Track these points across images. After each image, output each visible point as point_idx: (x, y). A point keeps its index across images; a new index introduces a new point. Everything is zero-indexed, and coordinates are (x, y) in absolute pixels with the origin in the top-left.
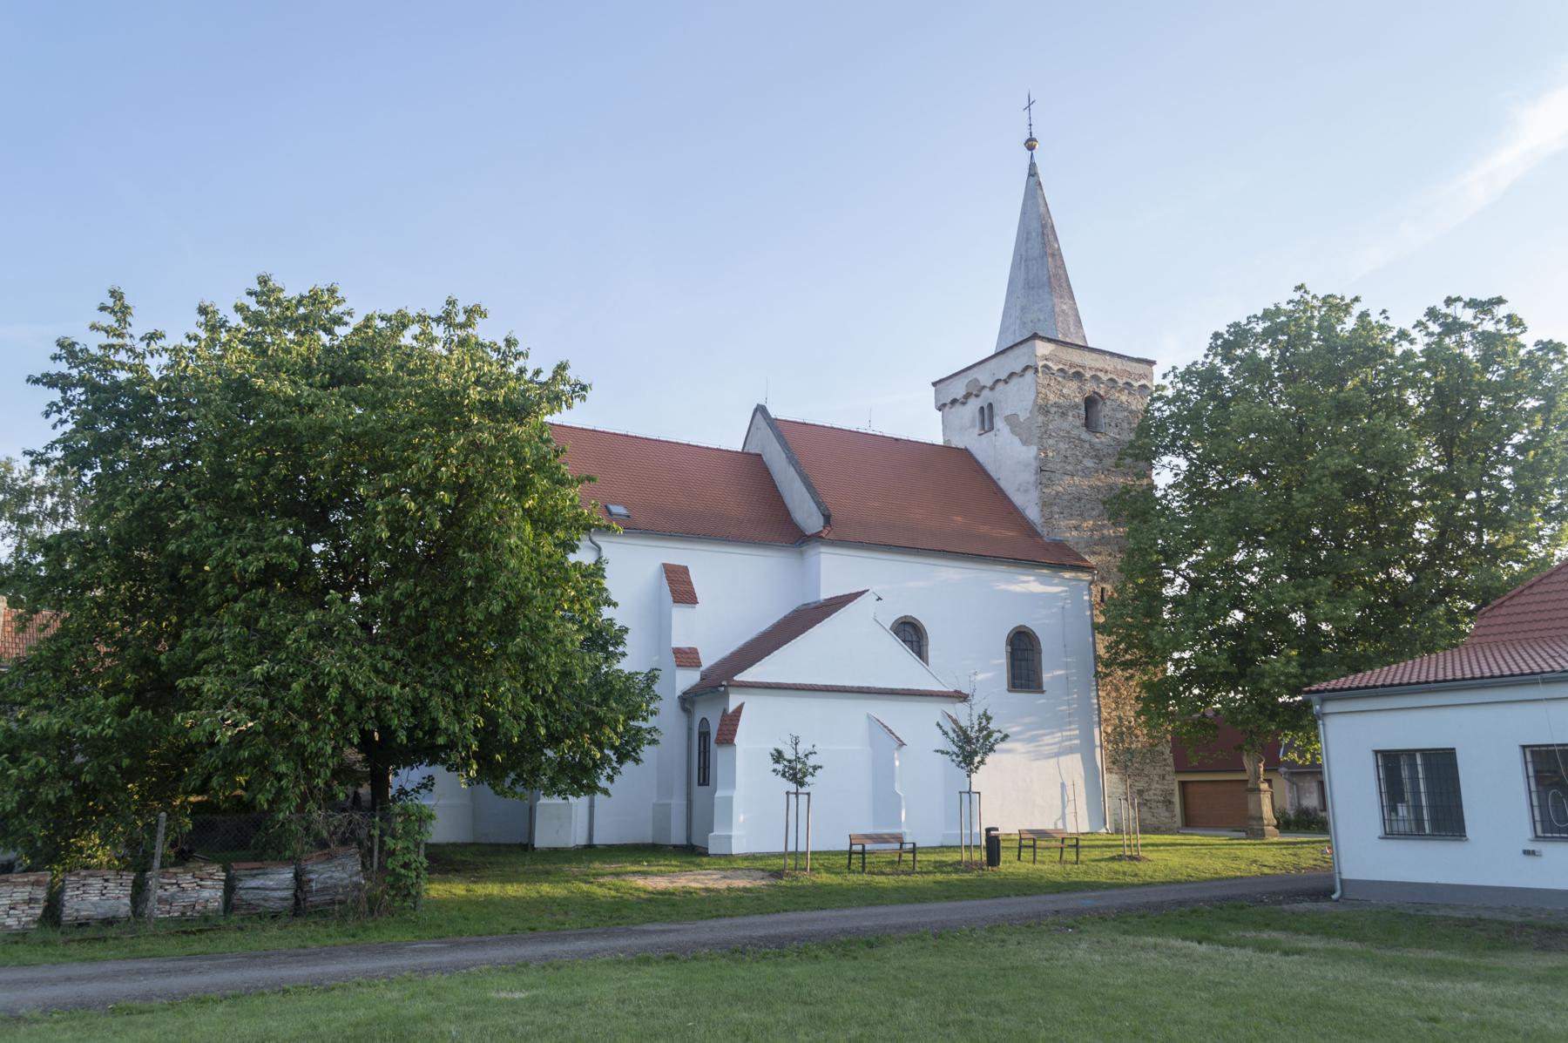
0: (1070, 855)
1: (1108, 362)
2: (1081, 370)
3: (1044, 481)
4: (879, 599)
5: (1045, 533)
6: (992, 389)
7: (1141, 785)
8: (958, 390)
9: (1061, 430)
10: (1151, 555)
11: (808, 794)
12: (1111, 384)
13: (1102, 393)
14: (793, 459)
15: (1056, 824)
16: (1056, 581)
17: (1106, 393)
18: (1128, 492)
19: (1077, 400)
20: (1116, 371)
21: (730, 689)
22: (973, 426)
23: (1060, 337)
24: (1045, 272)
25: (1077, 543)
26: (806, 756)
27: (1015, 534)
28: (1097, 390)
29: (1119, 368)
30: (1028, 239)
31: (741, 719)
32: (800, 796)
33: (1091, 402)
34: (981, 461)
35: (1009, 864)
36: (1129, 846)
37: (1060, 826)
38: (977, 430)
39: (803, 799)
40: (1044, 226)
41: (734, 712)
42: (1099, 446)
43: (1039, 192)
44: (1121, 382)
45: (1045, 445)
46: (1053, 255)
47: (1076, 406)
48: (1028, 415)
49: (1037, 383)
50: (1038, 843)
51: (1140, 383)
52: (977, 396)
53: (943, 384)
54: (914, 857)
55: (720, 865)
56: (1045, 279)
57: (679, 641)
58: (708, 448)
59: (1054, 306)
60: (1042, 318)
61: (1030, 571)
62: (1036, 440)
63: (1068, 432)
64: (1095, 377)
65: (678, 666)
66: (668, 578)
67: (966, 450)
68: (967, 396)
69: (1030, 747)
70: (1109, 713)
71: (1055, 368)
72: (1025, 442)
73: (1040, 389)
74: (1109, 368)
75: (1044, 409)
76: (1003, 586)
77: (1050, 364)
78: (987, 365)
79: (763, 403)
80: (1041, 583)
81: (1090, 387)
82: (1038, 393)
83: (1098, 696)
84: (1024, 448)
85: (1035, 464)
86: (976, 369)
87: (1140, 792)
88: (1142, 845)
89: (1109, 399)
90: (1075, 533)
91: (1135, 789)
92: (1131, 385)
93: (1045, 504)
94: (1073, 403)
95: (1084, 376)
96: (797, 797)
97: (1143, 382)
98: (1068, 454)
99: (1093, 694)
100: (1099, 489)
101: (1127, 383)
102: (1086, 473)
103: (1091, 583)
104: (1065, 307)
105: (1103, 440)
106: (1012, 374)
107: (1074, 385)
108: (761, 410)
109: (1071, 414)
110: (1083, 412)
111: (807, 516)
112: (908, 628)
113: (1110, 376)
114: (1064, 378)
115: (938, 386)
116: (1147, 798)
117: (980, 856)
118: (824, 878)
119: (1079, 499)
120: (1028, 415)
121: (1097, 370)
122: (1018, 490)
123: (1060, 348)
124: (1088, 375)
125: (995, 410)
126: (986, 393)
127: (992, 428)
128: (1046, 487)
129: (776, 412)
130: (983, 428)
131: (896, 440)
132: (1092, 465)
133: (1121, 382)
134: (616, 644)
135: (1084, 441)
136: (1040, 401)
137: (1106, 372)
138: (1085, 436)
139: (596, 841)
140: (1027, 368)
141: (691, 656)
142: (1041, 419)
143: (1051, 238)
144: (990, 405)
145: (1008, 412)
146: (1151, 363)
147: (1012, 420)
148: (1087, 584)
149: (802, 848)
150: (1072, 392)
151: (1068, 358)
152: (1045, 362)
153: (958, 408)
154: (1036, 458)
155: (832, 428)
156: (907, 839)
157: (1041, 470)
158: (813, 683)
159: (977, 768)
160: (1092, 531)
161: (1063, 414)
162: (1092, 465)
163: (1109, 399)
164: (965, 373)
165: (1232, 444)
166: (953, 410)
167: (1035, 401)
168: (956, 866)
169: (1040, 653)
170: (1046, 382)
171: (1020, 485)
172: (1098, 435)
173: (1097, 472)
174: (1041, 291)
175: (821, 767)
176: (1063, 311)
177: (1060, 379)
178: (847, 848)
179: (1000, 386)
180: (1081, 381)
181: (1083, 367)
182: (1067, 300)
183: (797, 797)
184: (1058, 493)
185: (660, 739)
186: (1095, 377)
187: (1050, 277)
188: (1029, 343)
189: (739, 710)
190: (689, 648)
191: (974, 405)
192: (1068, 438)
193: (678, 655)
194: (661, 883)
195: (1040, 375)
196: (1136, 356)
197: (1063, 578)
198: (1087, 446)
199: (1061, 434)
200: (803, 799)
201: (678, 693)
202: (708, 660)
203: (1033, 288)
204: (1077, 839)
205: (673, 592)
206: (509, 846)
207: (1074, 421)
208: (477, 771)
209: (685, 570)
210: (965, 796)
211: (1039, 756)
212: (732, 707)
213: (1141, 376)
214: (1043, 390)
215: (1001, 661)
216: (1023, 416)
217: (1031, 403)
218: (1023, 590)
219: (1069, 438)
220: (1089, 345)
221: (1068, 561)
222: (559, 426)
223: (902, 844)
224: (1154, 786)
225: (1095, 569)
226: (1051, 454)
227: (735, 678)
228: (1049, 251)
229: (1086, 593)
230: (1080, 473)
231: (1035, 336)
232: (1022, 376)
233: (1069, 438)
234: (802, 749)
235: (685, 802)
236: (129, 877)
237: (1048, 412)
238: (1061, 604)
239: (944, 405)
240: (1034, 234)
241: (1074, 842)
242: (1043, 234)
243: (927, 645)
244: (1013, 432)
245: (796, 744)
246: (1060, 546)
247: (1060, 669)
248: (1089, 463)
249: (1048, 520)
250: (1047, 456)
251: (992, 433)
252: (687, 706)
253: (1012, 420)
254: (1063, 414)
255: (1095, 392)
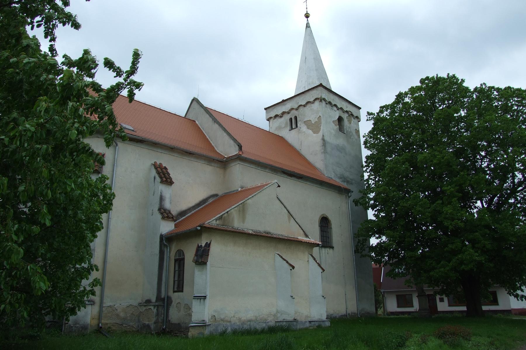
4: (279, 186)
6: (297, 109)
38: (289, 128)
122: (312, 154)
126: (294, 112)
144: (296, 118)
165: (429, 133)
179: (301, 109)
191: (287, 117)
236: (312, 322)
239: (271, 118)
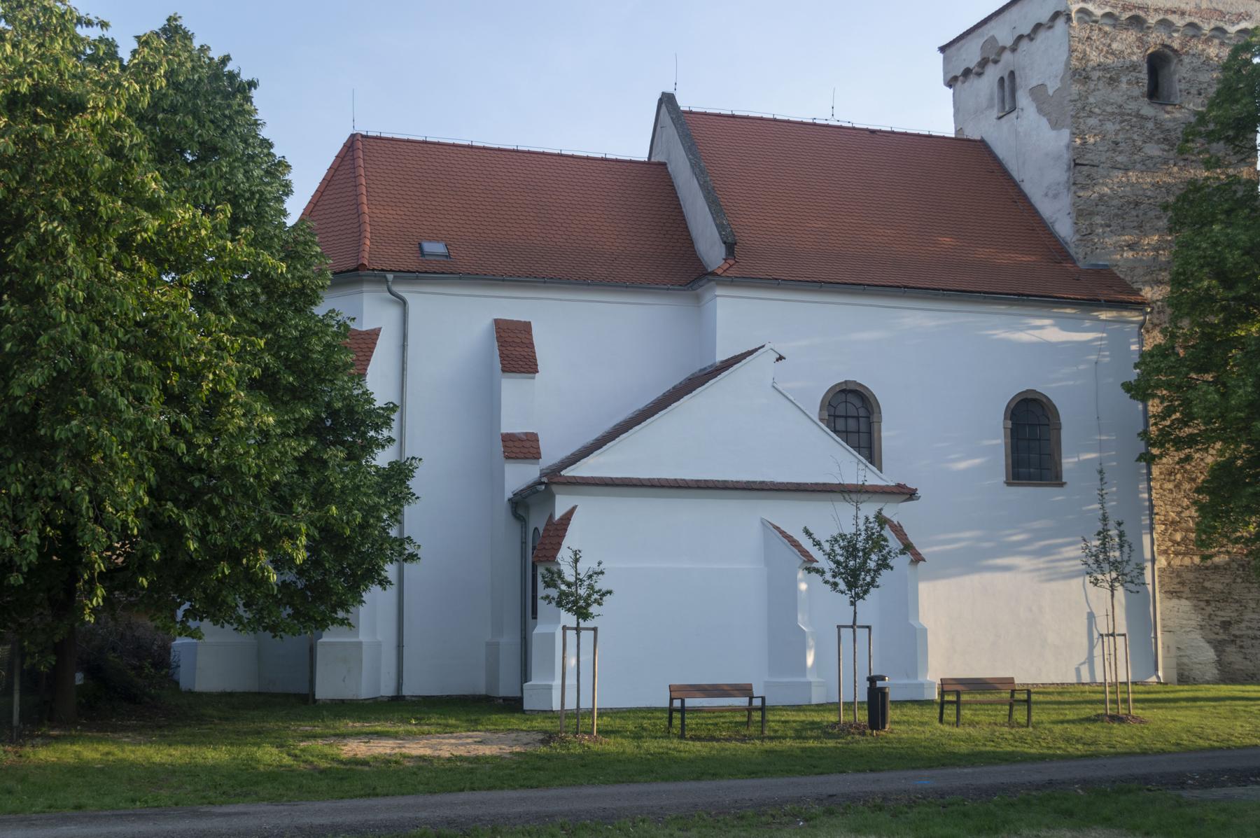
0: (1020, 715)
2: (1141, 13)
3: (1080, 180)
4: (781, 358)
5: (1081, 257)
6: (1014, 49)
7: (1228, 613)
8: (971, 55)
9: (1108, 104)
11: (595, 629)
12: (1191, 32)
13: (1176, 45)
14: (698, 169)
15: (1078, 670)
16: (1088, 324)
17: (1183, 45)
18: (1198, 189)
19: (1135, 58)
21: (554, 488)
22: (990, 106)
25: (1132, 269)
26: (590, 577)
27: (1033, 258)
28: (1168, 42)
31: (570, 528)
32: (583, 633)
33: (1158, 63)
34: (1001, 157)
35: (899, 727)
36: (1112, 702)
37: (1086, 678)
38: (995, 113)
39: (587, 636)
41: (561, 519)
42: (1171, 125)
44: (1207, 28)
45: (1082, 127)
47: (1134, 67)
49: (1070, 37)
50: (964, 698)
51: (1238, 28)
52: (996, 62)
53: (953, 49)
54: (763, 716)
55: (334, 728)
57: (511, 424)
58: (588, 158)
61: (1045, 311)
62: (1069, 121)
63: (1120, 106)
64: (1164, 23)
65: (507, 458)
66: (499, 339)
67: (982, 142)
68: (984, 63)
69: (1040, 562)
70: (1179, 514)
71: (1098, 12)
72: (1055, 125)
73: (1075, 44)
74: (1187, 8)
75: (1080, 75)
79: (670, 90)
80: (1064, 329)
81: (1155, 39)
82: (1072, 51)
83: (1150, 489)
84: (1054, 133)
85: (1066, 156)
87: (1226, 625)
88: (1135, 701)
90: (1129, 254)
91: (1218, 620)
93: (1082, 213)
94: (1128, 64)
95: (1145, 21)
96: (578, 634)
98: (1120, 137)
99: (1143, 486)
100: (1168, 188)
102: (1149, 165)
103: (1142, 325)
105: (1178, 115)
106: (1038, 26)
107: (1131, 36)
108: (667, 101)
109: (1124, 79)
110: (1144, 76)
111: (711, 249)
112: (851, 398)
113: (1188, 19)
114: (1114, 26)
116: (1237, 633)
117: (862, 716)
118: (611, 745)
119: (1137, 204)
120: (1059, 85)
121: (1167, 11)
124: (1152, 20)
125: (1018, 80)
126: (1007, 56)
127: (1013, 109)
128: (1083, 188)
129: (684, 103)
130: (1004, 107)
131: (873, 132)
133: (1207, 28)
134: (377, 428)
135: (1147, 119)
136: (1074, 62)
137: (1183, 13)
138: (1148, 110)
139: (406, 692)
140: (1056, 15)
141: (527, 444)
142: (1076, 88)
144: (1012, 74)
145: (1034, 83)
147: (1038, 93)
149: (586, 704)
150: (1127, 45)
154: (1068, 147)
156: (757, 692)
157: (1076, 164)
158: (678, 477)
159: (866, 592)
161: (1113, 81)
164: (980, 30)
167: (1068, 63)
168: (827, 731)
169: (1059, 429)
170: (1084, 34)
172: (1169, 108)
175: (610, 592)
177: (1107, 29)
178: (667, 704)
179: (1024, 44)
180: (1142, 30)
181: (1145, 9)
183: (578, 634)
184: (1102, 196)
185: (420, 553)
186: (1164, 23)
189: (567, 517)
190: (526, 434)
191: (993, 74)
192: (1121, 114)
193: (510, 444)
194: (383, 748)
195: (1075, 23)
197: (1098, 319)
198: (1150, 125)
199: (1109, 109)
200: (587, 636)
201: (508, 494)
202: (551, 454)
204: (1029, 692)
205: (503, 357)
206: (287, 696)
207: (1131, 91)
208: (104, 599)
209: (526, 327)
210: (847, 634)
211: (1054, 575)
212: (559, 513)
214: (1080, 48)
215: (996, 441)
217: (1062, 66)
218: (1034, 339)
219: (1122, 114)
221: (1104, 294)
222: (376, 138)
223: (751, 698)
224: (1249, 615)
225: (1148, 304)
227: (562, 473)
230: (1138, 166)
232: (1050, 27)
234: (583, 567)
235: (519, 640)
237: (1087, 78)
238: (1094, 357)
239: (955, 79)
241: (1025, 697)
243: (880, 422)
244: (1040, 111)
245: (576, 561)
246: (1104, 274)
247: (1095, 452)
248: (1153, 150)
249: (1086, 236)
250: (1084, 143)
251: (1013, 115)
252: (521, 512)
253: (1038, 93)
254: (1113, 81)
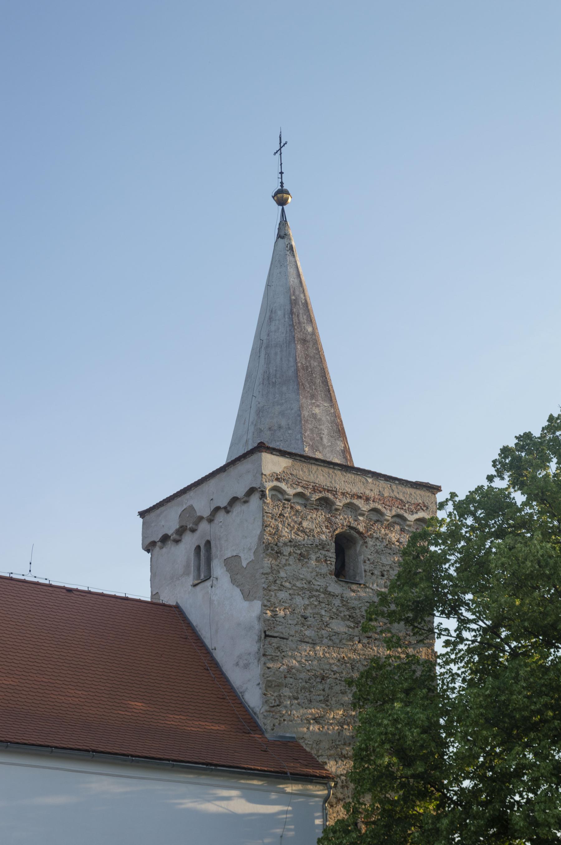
1: (371, 486)
2: (330, 496)
3: (270, 651)
5: (269, 728)
6: (210, 520)
10: (382, 756)
13: (361, 528)
16: (273, 796)
17: (368, 529)
19: (323, 537)
20: (381, 498)
22: (186, 573)
23: (307, 451)
24: (292, 363)
25: (318, 742)
27: (223, 727)
28: (354, 524)
29: (386, 495)
30: (271, 319)
38: (191, 580)
40: (293, 303)
42: (356, 603)
43: (290, 258)
44: (389, 514)
45: (273, 600)
46: (304, 341)
47: (322, 546)
48: (252, 557)
49: (264, 513)
51: (416, 516)
52: (193, 531)
53: (153, 515)
56: (291, 373)
59: (301, 408)
60: (283, 423)
62: (261, 593)
64: (350, 506)
67: (177, 607)
68: (181, 531)
71: (291, 491)
72: (247, 596)
73: (268, 520)
74: (371, 495)
76: (189, 804)
77: (283, 486)
78: (205, 487)
80: (251, 800)
82: (265, 526)
85: (257, 627)
86: (191, 493)
89: (371, 536)
90: (315, 728)
92: (404, 519)
95: (333, 503)
97: (421, 515)
101: (398, 516)
103: (326, 799)
104: (317, 411)
105: (362, 594)
106: (234, 500)
107: (320, 516)
109: (313, 557)
110: (332, 555)
113: (372, 505)
115: (147, 517)
119: (323, 678)
120: (252, 557)
121: (353, 496)
122: (237, 664)
123: (298, 465)
124: (339, 503)
125: (214, 550)
126: (204, 526)
127: (208, 577)
128: (273, 660)
131: (70, 590)
132: (344, 629)
133: (389, 514)
135: (334, 596)
136: (267, 537)
137: (367, 499)
138: (335, 587)
140: (252, 491)
142: (268, 562)
143: (303, 319)
144: (208, 543)
145: (229, 554)
146: (438, 489)
148: (320, 801)
151: (312, 478)
152: (275, 483)
153: (171, 547)
154: (259, 618)
155: (89, 592)
157: (266, 636)
160: (341, 724)
161: (303, 558)
162: (344, 629)
163: (371, 536)
166: (164, 550)
167: (261, 537)
170: (276, 511)
171: (240, 657)
172: (354, 587)
173: (351, 639)
174: (284, 389)
176: (314, 416)
177: (298, 507)
179: (221, 516)
181: (334, 492)
182: (320, 402)
184: (290, 669)
186: (350, 506)
187: (297, 370)
188: (254, 457)
195: (269, 500)
196: (413, 478)
197: (284, 792)
198: (337, 602)
199: (299, 584)
203: (274, 384)
213: (420, 507)
216: (246, 558)
217: (256, 539)
218: (221, 810)
219: (311, 590)
220: (356, 465)
221: (290, 767)
225: (333, 779)
226: (282, 613)
228: (298, 335)
229: (319, 814)
230: (325, 641)
231: (261, 447)
232: (246, 502)
233: (311, 590)
237: (279, 553)
238: (279, 831)
239: (153, 544)
240: (280, 313)
242: (292, 313)
244: (233, 581)
248: (339, 626)
250: (275, 616)
251: (208, 583)
254: (303, 558)
255: (351, 528)
